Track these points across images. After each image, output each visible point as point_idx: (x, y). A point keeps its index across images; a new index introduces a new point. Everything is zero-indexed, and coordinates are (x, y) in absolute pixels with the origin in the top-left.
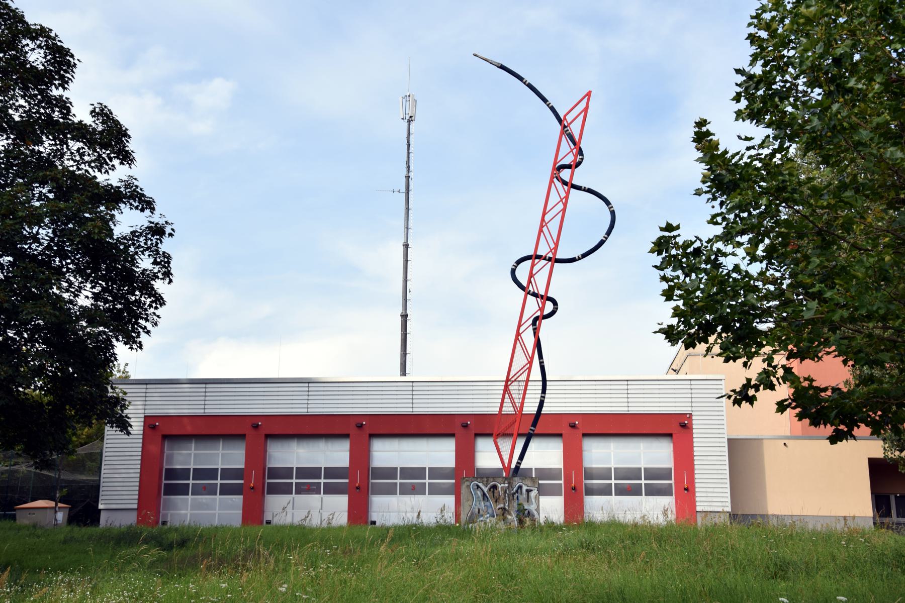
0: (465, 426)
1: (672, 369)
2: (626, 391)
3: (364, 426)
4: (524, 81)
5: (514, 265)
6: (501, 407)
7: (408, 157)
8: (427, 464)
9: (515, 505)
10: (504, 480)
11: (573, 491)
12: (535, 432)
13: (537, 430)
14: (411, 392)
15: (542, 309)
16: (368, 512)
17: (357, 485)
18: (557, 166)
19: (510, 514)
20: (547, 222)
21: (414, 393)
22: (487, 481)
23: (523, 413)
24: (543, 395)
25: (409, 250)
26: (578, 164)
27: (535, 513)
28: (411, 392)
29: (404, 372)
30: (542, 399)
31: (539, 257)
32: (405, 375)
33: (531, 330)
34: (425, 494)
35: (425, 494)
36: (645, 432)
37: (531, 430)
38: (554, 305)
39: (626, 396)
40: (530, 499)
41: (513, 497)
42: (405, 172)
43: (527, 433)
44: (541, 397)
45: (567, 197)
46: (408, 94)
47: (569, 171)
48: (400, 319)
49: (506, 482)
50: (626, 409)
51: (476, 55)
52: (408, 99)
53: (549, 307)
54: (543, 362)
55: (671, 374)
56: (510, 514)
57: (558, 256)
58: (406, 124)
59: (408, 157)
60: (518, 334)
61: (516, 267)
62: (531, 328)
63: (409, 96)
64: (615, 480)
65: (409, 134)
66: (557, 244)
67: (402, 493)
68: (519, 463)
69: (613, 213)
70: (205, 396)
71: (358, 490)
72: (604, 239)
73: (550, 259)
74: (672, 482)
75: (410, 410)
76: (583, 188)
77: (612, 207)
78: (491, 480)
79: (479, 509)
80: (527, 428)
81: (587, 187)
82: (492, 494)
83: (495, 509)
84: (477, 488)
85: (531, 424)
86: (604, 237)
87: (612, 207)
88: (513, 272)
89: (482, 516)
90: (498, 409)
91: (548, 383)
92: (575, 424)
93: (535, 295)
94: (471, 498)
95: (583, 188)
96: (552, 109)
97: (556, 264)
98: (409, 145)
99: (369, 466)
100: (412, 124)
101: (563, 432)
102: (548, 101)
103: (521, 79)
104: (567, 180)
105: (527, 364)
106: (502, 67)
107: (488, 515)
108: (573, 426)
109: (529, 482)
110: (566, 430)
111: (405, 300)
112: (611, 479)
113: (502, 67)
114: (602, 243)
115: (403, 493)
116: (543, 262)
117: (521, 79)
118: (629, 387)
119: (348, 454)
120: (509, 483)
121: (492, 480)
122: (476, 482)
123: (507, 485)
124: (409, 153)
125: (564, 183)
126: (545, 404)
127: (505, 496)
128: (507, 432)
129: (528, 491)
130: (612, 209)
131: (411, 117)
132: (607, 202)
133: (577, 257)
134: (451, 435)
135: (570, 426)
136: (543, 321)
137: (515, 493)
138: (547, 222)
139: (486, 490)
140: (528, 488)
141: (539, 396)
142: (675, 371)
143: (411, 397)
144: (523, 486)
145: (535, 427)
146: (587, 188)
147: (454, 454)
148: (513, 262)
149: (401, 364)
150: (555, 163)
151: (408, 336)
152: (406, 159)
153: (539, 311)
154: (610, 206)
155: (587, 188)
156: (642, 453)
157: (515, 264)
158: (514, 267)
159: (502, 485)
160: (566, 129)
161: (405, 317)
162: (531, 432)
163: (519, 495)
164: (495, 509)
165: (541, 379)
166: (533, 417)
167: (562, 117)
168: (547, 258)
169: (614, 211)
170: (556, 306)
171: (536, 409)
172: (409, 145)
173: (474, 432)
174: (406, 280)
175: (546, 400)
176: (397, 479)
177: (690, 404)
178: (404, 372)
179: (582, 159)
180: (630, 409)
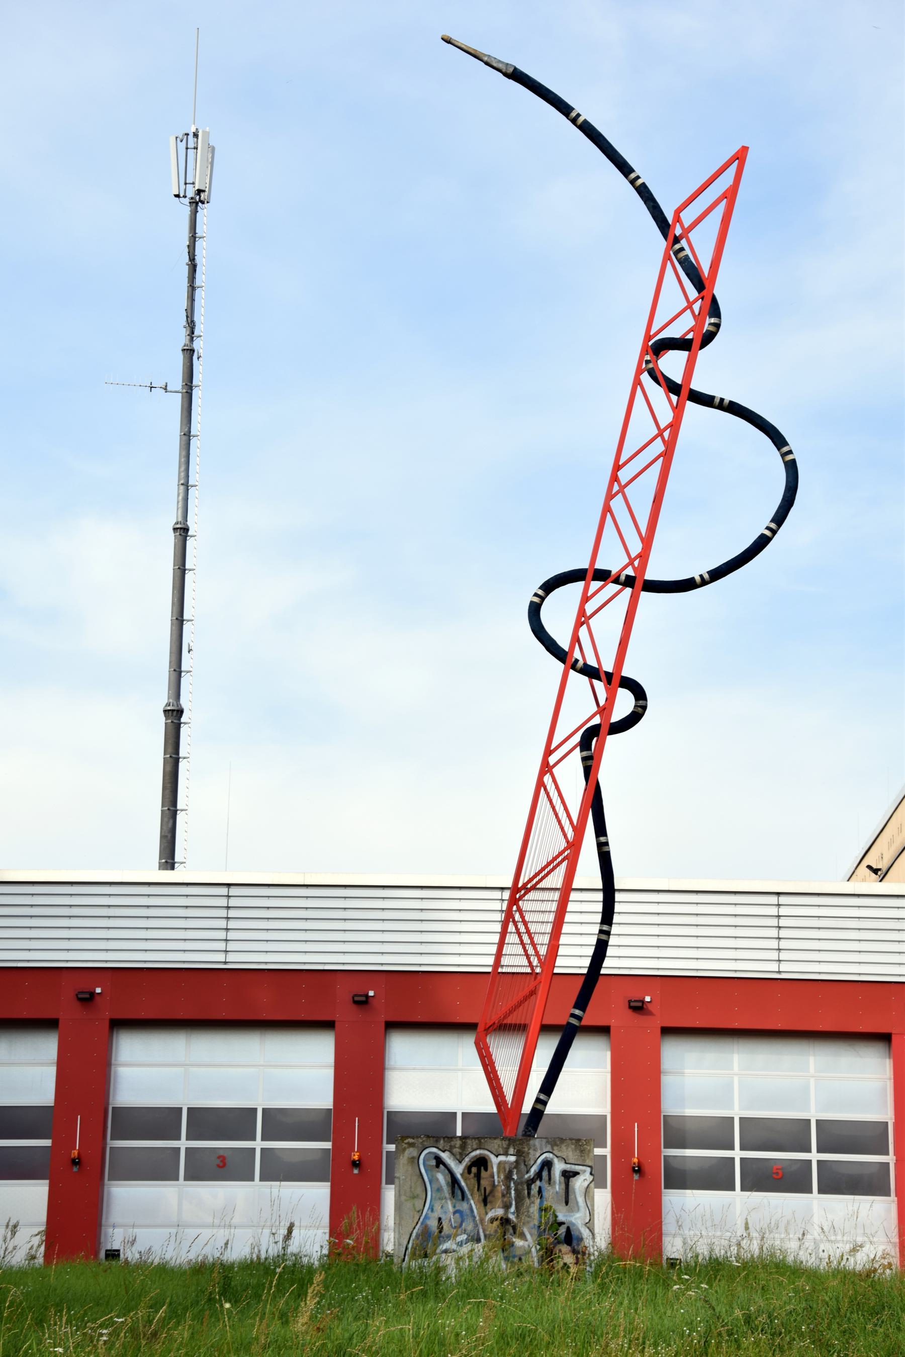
0: (362, 1002)
1: (869, 867)
2: (774, 922)
3: (97, 998)
4: (573, 114)
5: (536, 595)
6: (499, 955)
7: (191, 299)
8: (260, 1101)
9: (534, 1209)
10: (505, 1144)
11: (636, 1177)
12: (584, 1022)
13: (590, 1018)
14: (223, 913)
15: (605, 710)
16: (100, 1225)
17: (75, 1153)
18: (650, 343)
19: (522, 1236)
20: (623, 483)
21: (232, 913)
22: (463, 1147)
23: (556, 971)
24: (605, 928)
25: (190, 543)
26: (708, 338)
27: (585, 1233)
28: (223, 913)
29: (168, 860)
30: (604, 937)
31: (603, 576)
32: (173, 868)
33: (576, 759)
34: (252, 1179)
35: (252, 1179)
36: (820, 1028)
37: (573, 1015)
38: (637, 699)
39: (774, 933)
40: (571, 1197)
41: (529, 1189)
42: (182, 339)
43: (565, 1023)
44: (601, 931)
45: (675, 426)
46: (193, 130)
47: (683, 355)
48: (162, 719)
49: (511, 1151)
50: (774, 967)
51: (448, 41)
52: (191, 144)
53: (625, 703)
54: (607, 844)
55: (864, 880)
56: (522, 1236)
57: (651, 575)
58: (187, 210)
59: (191, 299)
60: (546, 768)
61: (543, 599)
62: (577, 754)
63: (196, 135)
64: (819, 1151)
65: (193, 238)
66: (647, 541)
67: (192, 1176)
68: (541, 1102)
69: (792, 468)
70: (227, 929)
71: (75, 1169)
72: (768, 533)
73: (629, 582)
74: (890, 1159)
75: (221, 957)
76: (717, 401)
77: (790, 452)
78: (472, 1144)
79: (440, 1219)
80: (563, 1014)
81: (728, 397)
82: (474, 1182)
83: (482, 1220)
84: (437, 1166)
85: (573, 1006)
86: (768, 528)
87: (790, 452)
88: (534, 611)
89: (449, 1237)
90: (491, 961)
91: (618, 897)
92: (643, 1002)
93: (591, 672)
94: (419, 1190)
95: (717, 401)
96: (644, 192)
97: (645, 596)
98: (193, 268)
99: (108, 1104)
100: (204, 212)
101: (613, 1023)
102: (632, 171)
103: (564, 108)
104: (678, 379)
105: (565, 849)
106: (518, 76)
107: (464, 1237)
108: (638, 1008)
109: (569, 1152)
110: (68, 1010)
111: (177, 672)
112: (732, 1148)
113: (518, 76)
114: (761, 543)
115: (826, 1188)
116: (613, 588)
117: (564, 108)
118: (783, 911)
119: (52, 1071)
120: (519, 1154)
121: (475, 1143)
122: (434, 1150)
123: (513, 1159)
124: (192, 288)
125: (672, 387)
126: (610, 951)
127: (508, 1188)
128: (509, 1021)
129: (568, 1175)
130: (790, 457)
131: (199, 192)
132: (778, 440)
133: (698, 579)
134: (326, 1025)
135: (630, 1007)
136: (610, 738)
137: (533, 1181)
138: (623, 483)
139: (458, 1169)
140: (568, 1167)
141: (596, 929)
142: (876, 871)
143: (222, 924)
144: (556, 1160)
145: (583, 1010)
146: (726, 402)
147: (330, 1073)
148: (535, 587)
149: (162, 837)
150: (648, 337)
151: (182, 765)
152: (184, 304)
153: (598, 716)
154: (785, 449)
155: (726, 402)
156: (812, 1081)
157: (540, 592)
158: (536, 600)
159: (502, 1158)
160: (677, 247)
161: (174, 715)
162: (574, 1021)
163: (544, 1184)
164: (482, 1220)
165: (600, 886)
166: (580, 982)
167: (670, 217)
168: (623, 578)
169: (794, 462)
170: (641, 703)
171: (587, 962)
172: (193, 268)
173: (383, 1018)
174: (179, 620)
175: (612, 941)
176: (254, 1139)
177: (774, 955)
178: (168, 860)
179: (718, 326)
180: (784, 967)
